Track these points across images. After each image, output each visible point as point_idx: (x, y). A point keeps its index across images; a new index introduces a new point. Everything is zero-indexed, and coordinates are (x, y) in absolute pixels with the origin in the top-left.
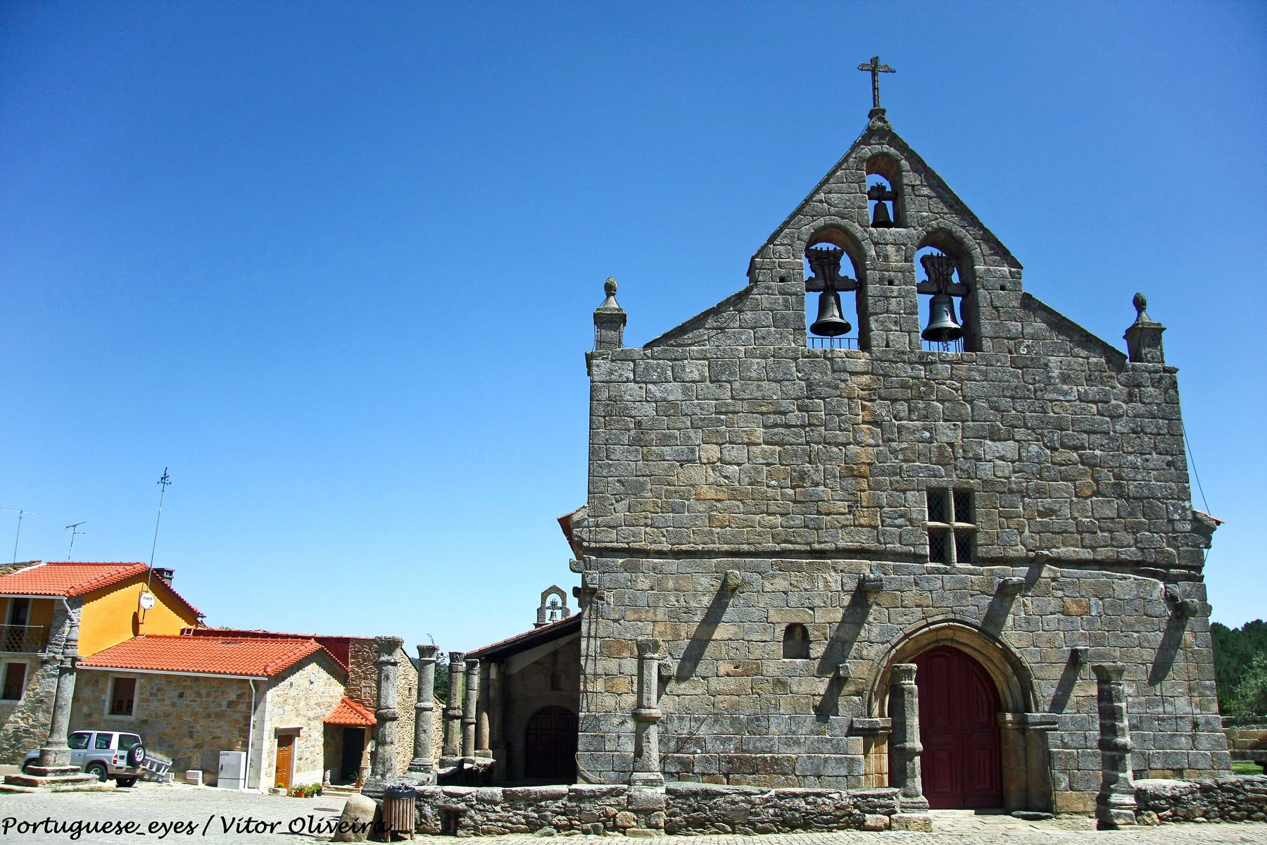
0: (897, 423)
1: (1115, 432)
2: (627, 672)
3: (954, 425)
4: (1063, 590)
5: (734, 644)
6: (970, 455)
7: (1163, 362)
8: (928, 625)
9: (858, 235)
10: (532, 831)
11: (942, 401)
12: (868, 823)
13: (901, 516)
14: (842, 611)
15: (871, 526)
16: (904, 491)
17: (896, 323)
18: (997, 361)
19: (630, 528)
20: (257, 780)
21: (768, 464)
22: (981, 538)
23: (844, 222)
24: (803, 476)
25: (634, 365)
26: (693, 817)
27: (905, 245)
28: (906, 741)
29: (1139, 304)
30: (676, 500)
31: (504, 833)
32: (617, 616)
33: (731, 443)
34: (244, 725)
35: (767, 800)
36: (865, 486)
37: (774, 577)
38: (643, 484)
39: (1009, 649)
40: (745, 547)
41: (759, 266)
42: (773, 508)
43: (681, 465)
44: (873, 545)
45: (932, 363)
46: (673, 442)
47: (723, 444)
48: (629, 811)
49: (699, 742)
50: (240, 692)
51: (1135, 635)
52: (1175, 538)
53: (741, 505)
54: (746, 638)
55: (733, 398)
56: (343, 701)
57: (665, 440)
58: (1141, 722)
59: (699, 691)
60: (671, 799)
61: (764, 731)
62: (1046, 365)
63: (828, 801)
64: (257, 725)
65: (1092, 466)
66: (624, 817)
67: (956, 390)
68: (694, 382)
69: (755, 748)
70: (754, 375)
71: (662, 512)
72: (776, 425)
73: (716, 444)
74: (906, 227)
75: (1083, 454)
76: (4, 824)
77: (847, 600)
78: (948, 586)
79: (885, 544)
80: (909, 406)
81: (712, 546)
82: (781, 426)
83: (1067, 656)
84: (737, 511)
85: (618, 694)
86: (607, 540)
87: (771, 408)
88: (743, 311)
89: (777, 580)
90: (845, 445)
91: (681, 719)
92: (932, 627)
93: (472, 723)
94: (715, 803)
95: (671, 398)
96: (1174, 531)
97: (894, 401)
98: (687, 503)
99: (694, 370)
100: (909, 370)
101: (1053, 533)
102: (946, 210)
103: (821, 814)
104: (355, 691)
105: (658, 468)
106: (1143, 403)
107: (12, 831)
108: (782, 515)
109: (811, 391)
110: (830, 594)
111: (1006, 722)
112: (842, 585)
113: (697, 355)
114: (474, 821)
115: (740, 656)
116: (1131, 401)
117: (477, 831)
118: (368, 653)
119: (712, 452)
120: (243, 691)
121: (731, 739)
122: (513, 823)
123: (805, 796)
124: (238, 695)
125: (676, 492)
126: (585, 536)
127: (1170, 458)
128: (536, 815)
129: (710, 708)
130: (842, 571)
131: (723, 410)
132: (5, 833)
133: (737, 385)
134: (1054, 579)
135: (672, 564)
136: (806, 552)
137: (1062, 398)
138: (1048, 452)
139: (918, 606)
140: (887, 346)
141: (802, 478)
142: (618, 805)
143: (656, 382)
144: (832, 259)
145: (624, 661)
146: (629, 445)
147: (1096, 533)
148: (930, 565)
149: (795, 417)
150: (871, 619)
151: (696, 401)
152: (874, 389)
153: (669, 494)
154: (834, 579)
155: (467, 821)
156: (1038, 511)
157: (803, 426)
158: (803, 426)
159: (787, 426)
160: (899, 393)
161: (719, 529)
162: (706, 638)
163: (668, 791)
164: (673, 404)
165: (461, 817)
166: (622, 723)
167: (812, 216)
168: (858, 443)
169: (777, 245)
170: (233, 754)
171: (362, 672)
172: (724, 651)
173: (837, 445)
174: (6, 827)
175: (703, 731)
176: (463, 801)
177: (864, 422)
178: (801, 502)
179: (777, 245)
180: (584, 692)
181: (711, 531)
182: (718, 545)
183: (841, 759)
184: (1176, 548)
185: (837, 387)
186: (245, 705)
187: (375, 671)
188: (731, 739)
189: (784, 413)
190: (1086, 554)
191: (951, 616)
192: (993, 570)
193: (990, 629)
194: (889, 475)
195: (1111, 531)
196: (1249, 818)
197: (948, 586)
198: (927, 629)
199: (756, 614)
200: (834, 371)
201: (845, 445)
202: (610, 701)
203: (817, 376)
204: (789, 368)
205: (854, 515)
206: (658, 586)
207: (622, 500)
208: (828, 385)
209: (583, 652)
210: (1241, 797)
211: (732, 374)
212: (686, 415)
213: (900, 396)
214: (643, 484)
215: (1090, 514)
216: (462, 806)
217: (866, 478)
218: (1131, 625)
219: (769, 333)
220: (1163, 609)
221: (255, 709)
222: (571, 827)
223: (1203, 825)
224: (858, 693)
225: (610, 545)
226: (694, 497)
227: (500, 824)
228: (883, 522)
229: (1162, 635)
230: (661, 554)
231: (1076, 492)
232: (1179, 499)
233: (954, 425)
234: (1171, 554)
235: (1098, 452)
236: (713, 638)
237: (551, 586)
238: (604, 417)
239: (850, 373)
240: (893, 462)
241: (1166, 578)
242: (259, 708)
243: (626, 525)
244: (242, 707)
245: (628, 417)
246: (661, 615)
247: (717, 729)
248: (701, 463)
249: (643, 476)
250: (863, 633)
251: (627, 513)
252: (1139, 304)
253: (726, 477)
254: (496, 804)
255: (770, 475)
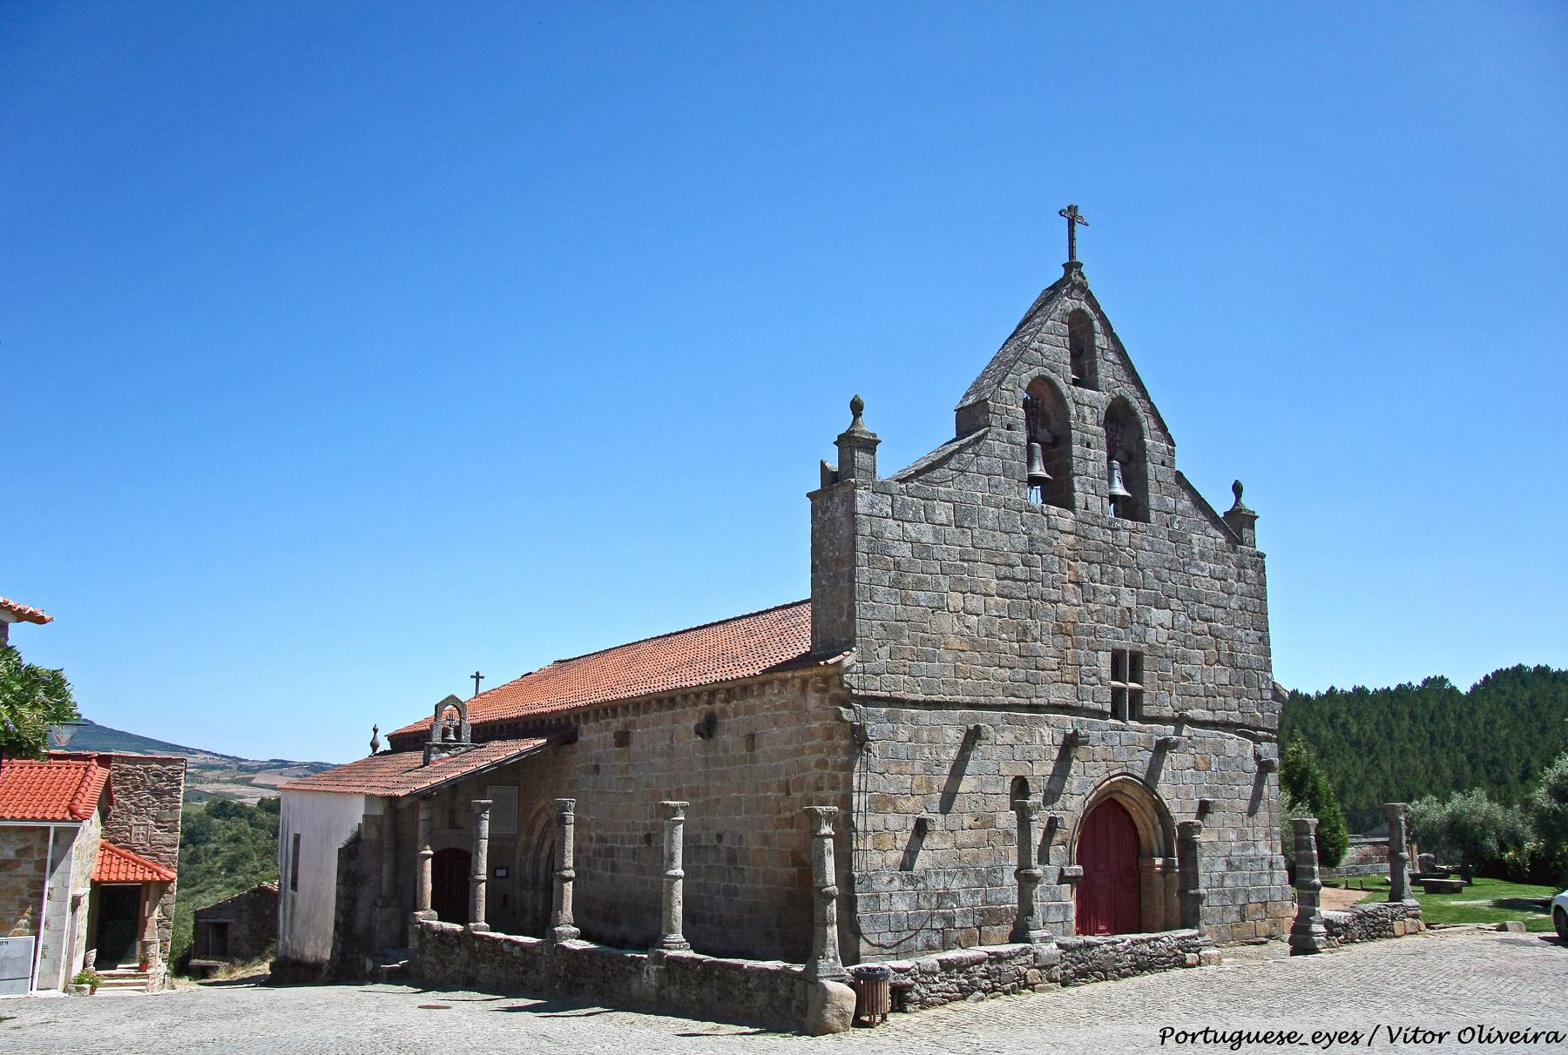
0: (1093, 584)
1: (1230, 608)
2: (891, 828)
3: (1132, 591)
4: (1195, 748)
5: (974, 797)
6: (1142, 621)
7: (1255, 547)
8: (1110, 777)
9: (1064, 391)
10: (964, 998)
11: (1123, 567)
12: (1189, 961)
13: (1094, 675)
14: (1052, 764)
15: (1073, 683)
16: (1096, 651)
17: (1093, 486)
18: (1160, 533)
19: (892, 676)
20: (54, 976)
21: (1000, 617)
22: (1146, 699)
23: (1053, 376)
24: (1026, 630)
25: (893, 499)
26: (1079, 968)
27: (1097, 409)
28: (1404, 898)
29: (857, 407)
30: (929, 649)
31: (945, 1003)
32: (882, 770)
33: (972, 592)
34: (30, 896)
35: (1126, 948)
36: (1069, 644)
37: (1003, 730)
38: (902, 629)
39: (1162, 800)
40: (982, 700)
41: (991, 410)
42: (1004, 662)
43: (933, 612)
44: (1073, 702)
45: (1118, 529)
46: (926, 587)
47: (966, 593)
48: (1036, 968)
49: (954, 896)
50: (22, 846)
51: (1237, 788)
52: (1262, 704)
53: (979, 657)
54: (984, 791)
55: (973, 546)
56: (103, 848)
57: (919, 585)
58: (1241, 863)
59: (948, 845)
60: (1064, 953)
61: (1000, 882)
62: (1190, 541)
63: (1163, 944)
64: (54, 894)
65: (1216, 637)
66: (1033, 974)
67: (1133, 557)
68: (942, 525)
69: (996, 899)
70: (989, 524)
71: (918, 660)
72: (1006, 578)
73: (961, 592)
74: (1098, 390)
75: (1211, 626)
76: (1162, 1034)
77: (1056, 753)
78: (1124, 742)
79: (1083, 701)
80: (1101, 569)
81: (957, 697)
82: (1009, 579)
83: (1197, 806)
84: (976, 662)
85: (884, 851)
86: (873, 688)
87: (1003, 560)
88: (980, 456)
89: (1005, 734)
90: (1056, 602)
91: (937, 874)
92: (1112, 780)
93: (483, 881)
94: (1094, 954)
95: (924, 540)
96: (1262, 699)
97: (1091, 563)
98: (938, 651)
99: (943, 512)
100: (1102, 535)
101: (1190, 696)
102: (1125, 379)
103: (1159, 956)
104: (119, 832)
105: (914, 613)
106: (1246, 583)
107: (1170, 1041)
108: (1010, 668)
109: (1032, 546)
110: (1044, 747)
111: (1154, 866)
112: (1053, 740)
113: (944, 497)
114: (920, 994)
115: (979, 810)
116: (1239, 581)
117: (924, 1004)
118: (140, 776)
119: (955, 600)
120: (29, 844)
121: (978, 892)
122: (951, 992)
123: (1148, 941)
124: (18, 852)
125: (929, 640)
126: (854, 683)
127: (1260, 634)
128: (966, 982)
129: (957, 862)
130: (1052, 726)
131: (966, 557)
132: (1162, 1043)
133: (976, 533)
134: (1190, 738)
135: (926, 716)
136: (1027, 706)
137: (1200, 573)
138: (1190, 621)
139: (1104, 760)
140: (1086, 508)
141: (1025, 633)
142: (1027, 963)
143: (911, 522)
144: (1034, 409)
145: (889, 817)
146: (889, 587)
147: (1215, 697)
148: (1112, 721)
149: (1020, 571)
150: (1072, 772)
151: (944, 546)
152: (1077, 550)
153: (924, 642)
154: (1047, 732)
155: (915, 996)
156: (1182, 676)
157: (1026, 581)
158: (1026, 581)
159: (1014, 579)
160: (1095, 556)
161: (962, 680)
162: (953, 792)
163: (1060, 946)
164: (926, 547)
165: (907, 992)
166: (891, 881)
167: (1030, 364)
168: (1065, 602)
169: (1003, 389)
170: (16, 941)
171: (131, 803)
172: (967, 805)
173: (1051, 601)
174: (1164, 1037)
175: (954, 886)
176: (908, 975)
177: (1070, 582)
178: (1023, 656)
179: (1003, 389)
180: (856, 850)
181: (957, 682)
182: (961, 697)
183: (1059, 906)
184: (1262, 713)
185: (1050, 545)
186: (32, 866)
187: (154, 802)
188: (978, 892)
189: (1012, 566)
190: (1208, 716)
191: (1125, 770)
192: (1152, 728)
193: (1151, 783)
194: (1087, 635)
195: (1225, 697)
196: (1380, 936)
197: (1124, 742)
198: (1109, 782)
199: (991, 768)
200: (1049, 528)
201: (1056, 602)
202: (876, 859)
203: (1036, 532)
204: (1015, 521)
205: (1062, 671)
206: (914, 737)
207: (884, 645)
208: (1044, 541)
209: (855, 808)
210: (1376, 921)
211: (973, 521)
212: (937, 559)
213: (1094, 559)
214: (902, 629)
215: (1213, 680)
216: (909, 980)
217: (1070, 636)
218: (1235, 780)
219: (1000, 482)
220: (1252, 766)
221: (53, 870)
222: (994, 989)
223: (1361, 945)
224: (1063, 843)
225: (875, 693)
226: (943, 646)
227: (940, 994)
228: (1081, 679)
229: (1252, 788)
230: (915, 704)
231: (1206, 660)
232: (1265, 671)
233: (1132, 591)
234: (1258, 718)
235: (1220, 625)
236: (959, 791)
237: (449, 695)
238: (868, 554)
239: (1060, 531)
240: (1089, 622)
241: (1257, 740)
242: (60, 868)
243: (888, 673)
244: (27, 869)
245: (888, 556)
246: (918, 768)
247: (965, 882)
248: (949, 611)
249: (902, 621)
250: (1067, 785)
251: (889, 660)
252: (857, 407)
253: (968, 627)
254: (935, 974)
255: (1001, 629)
